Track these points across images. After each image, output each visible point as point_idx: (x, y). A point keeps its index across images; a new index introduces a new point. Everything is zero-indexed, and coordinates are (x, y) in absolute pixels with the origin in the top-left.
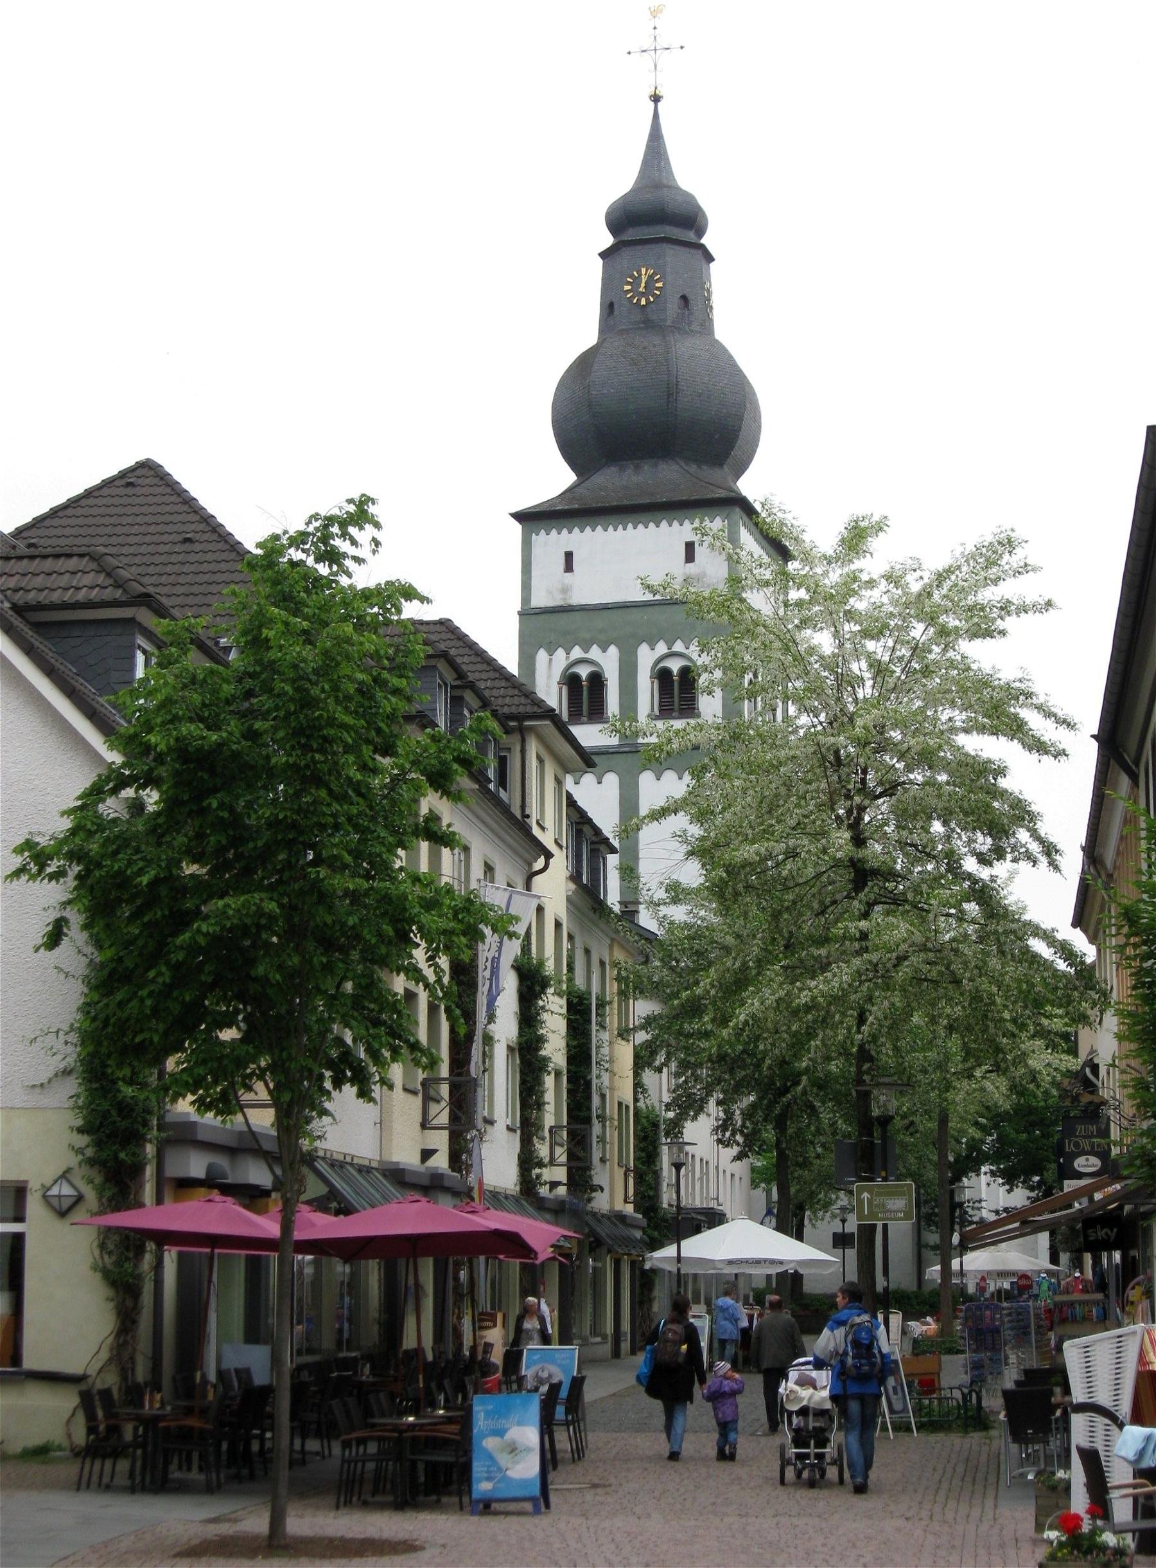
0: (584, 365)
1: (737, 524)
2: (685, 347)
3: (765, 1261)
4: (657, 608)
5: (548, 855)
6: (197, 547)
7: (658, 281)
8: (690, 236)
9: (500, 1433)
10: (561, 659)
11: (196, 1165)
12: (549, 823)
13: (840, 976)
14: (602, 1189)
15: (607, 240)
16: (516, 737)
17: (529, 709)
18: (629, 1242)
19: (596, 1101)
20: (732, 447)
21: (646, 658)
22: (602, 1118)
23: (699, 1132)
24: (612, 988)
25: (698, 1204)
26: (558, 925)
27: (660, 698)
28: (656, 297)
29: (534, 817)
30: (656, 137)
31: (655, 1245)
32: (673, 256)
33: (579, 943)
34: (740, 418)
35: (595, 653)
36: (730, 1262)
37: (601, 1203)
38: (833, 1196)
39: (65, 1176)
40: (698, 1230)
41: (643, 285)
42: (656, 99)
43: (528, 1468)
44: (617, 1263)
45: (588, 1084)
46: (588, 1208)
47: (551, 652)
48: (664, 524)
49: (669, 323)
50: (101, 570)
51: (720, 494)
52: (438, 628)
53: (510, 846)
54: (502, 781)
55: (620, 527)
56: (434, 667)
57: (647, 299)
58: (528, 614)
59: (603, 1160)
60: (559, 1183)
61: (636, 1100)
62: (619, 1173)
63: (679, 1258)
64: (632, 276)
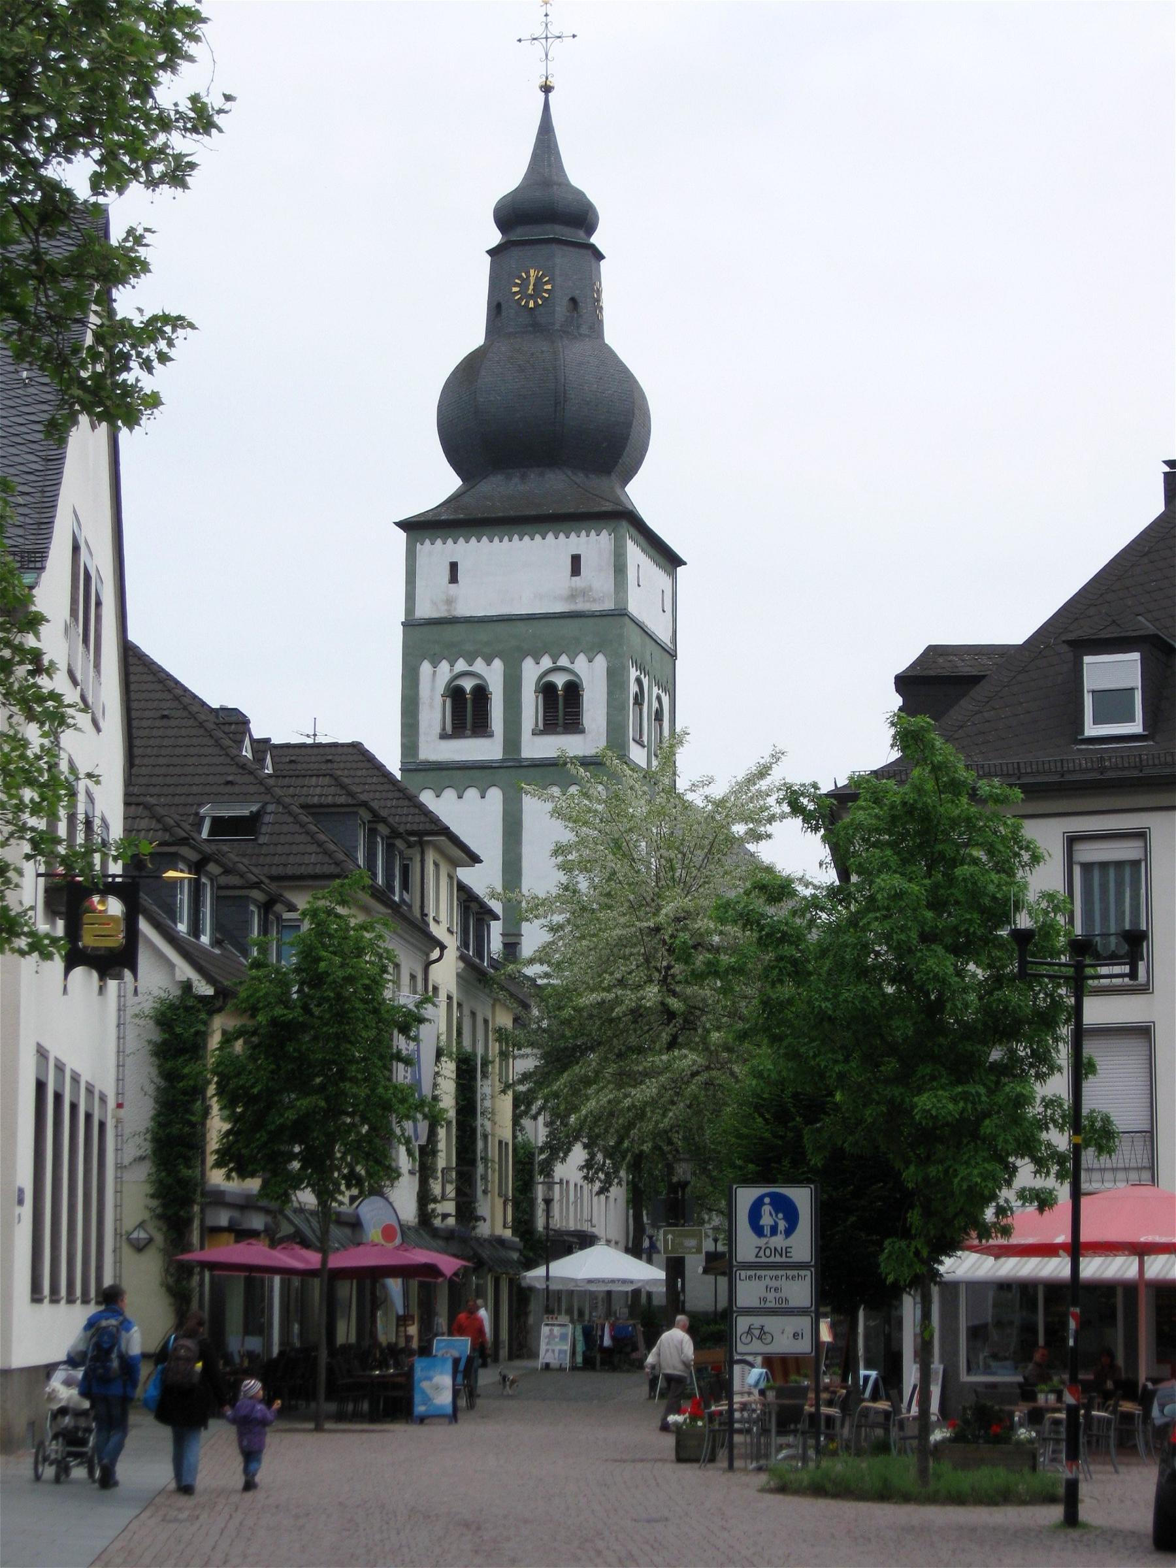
0: (470, 368)
1: (624, 537)
2: (574, 352)
3: (619, 1280)
4: (543, 622)
5: (443, 948)
6: (173, 723)
7: (546, 283)
8: (580, 235)
9: (430, 1379)
10: (445, 671)
11: (223, 1218)
12: (443, 916)
13: (648, 1090)
14: (485, 1220)
15: (495, 237)
16: (417, 849)
17: (428, 827)
18: (507, 1263)
19: (480, 1145)
20: (620, 456)
21: (531, 672)
22: (485, 1159)
23: (571, 1167)
24: (495, 1048)
25: (572, 1226)
26: (449, 998)
27: (545, 712)
28: (545, 299)
29: (432, 915)
30: (546, 130)
31: (530, 1265)
32: (562, 259)
33: (466, 1012)
34: (629, 425)
35: (479, 666)
36: (590, 1281)
37: (483, 1230)
38: (706, 1217)
39: (141, 1225)
40: (569, 1251)
41: (531, 287)
42: (547, 89)
43: (444, 1398)
44: (497, 1282)
45: (474, 1131)
46: (473, 1234)
47: (435, 666)
48: (550, 536)
49: (557, 327)
50: (153, 817)
51: (608, 507)
52: (350, 750)
53: (412, 944)
54: (405, 886)
55: (506, 538)
56: (356, 813)
57: (536, 302)
58: (411, 625)
59: (485, 1192)
60: (448, 1215)
61: (514, 1137)
62: (499, 1202)
63: (547, 1277)
64: (520, 277)
